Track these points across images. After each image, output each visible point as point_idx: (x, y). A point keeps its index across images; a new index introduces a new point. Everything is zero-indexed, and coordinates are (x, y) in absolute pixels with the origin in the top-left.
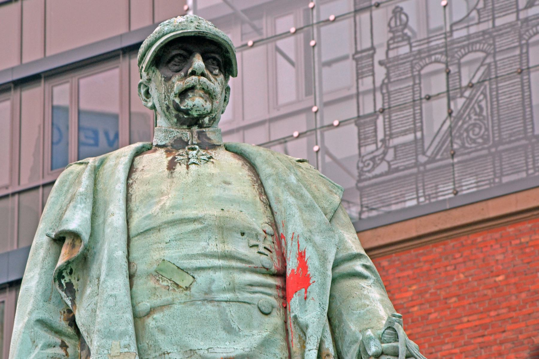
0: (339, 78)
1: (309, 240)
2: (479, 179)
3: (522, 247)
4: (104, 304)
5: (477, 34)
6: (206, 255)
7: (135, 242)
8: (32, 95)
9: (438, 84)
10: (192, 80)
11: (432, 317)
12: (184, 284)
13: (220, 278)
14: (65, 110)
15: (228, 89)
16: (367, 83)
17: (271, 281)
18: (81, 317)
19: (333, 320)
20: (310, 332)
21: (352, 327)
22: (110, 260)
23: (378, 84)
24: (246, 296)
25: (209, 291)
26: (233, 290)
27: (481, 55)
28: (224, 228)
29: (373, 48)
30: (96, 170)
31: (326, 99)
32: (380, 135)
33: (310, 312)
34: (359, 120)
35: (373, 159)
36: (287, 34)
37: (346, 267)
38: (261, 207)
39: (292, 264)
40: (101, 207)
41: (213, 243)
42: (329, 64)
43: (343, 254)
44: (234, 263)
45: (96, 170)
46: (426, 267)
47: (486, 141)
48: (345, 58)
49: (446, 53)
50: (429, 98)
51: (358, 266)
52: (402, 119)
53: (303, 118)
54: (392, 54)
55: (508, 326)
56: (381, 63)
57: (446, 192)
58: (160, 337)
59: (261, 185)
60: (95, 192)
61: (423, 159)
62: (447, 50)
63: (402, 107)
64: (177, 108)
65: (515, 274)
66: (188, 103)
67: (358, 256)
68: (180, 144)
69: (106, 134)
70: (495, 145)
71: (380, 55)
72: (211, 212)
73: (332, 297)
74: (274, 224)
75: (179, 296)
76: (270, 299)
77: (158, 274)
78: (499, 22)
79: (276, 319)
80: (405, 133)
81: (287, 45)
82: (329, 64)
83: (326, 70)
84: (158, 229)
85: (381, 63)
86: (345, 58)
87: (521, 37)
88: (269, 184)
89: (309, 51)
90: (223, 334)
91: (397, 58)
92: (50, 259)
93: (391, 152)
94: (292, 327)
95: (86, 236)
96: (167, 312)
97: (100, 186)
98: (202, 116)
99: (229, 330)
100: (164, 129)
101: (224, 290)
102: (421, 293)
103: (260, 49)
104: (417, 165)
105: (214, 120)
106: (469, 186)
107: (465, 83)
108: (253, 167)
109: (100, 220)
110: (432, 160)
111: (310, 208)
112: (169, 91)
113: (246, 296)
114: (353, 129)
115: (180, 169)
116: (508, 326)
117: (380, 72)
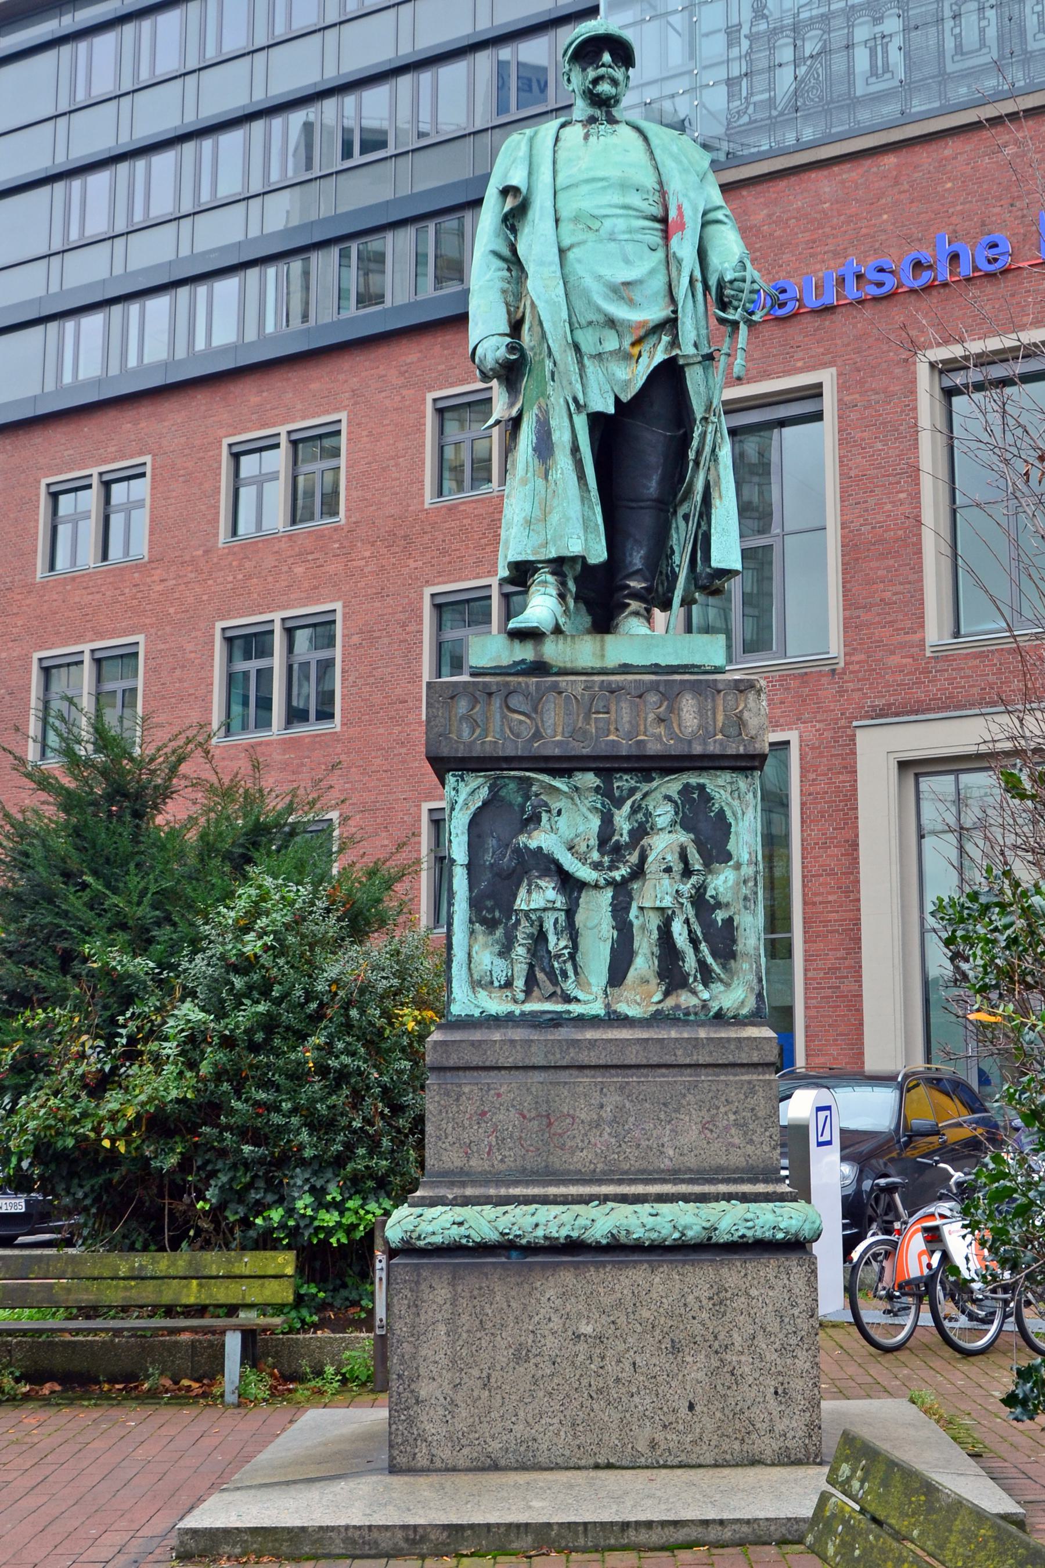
0: (714, 47)
1: (686, 195)
3: (843, 182)
4: (536, 242)
5: (817, 17)
6: (611, 206)
7: (559, 195)
8: (484, 59)
9: (787, 54)
10: (602, 71)
11: (777, 234)
12: (595, 227)
13: (621, 224)
14: (508, 63)
15: (628, 78)
16: (735, 52)
17: (658, 226)
18: (520, 252)
19: (702, 254)
20: (684, 264)
21: (715, 260)
22: (542, 207)
23: (743, 53)
24: (639, 237)
25: (612, 233)
26: (630, 232)
27: (820, 32)
28: (624, 186)
29: (740, 24)
30: (531, 140)
31: (704, 63)
32: (744, 94)
33: (685, 247)
34: (730, 82)
35: (738, 112)
36: (676, 11)
37: (711, 216)
38: (651, 170)
39: (673, 214)
40: (535, 167)
41: (616, 197)
42: (707, 35)
43: (708, 207)
44: (631, 212)
45: (531, 140)
46: (774, 196)
47: (821, 100)
48: (720, 31)
49: (794, 30)
50: (780, 65)
51: (719, 215)
52: (760, 81)
53: (686, 78)
54: (754, 30)
55: (829, 241)
56: (746, 37)
57: (790, 139)
58: (577, 266)
59: (652, 153)
60: (531, 156)
61: (774, 113)
62: (795, 28)
63: (760, 72)
64: (590, 91)
65: (837, 202)
67: (721, 207)
68: (592, 120)
69: (538, 81)
70: (828, 103)
71: (745, 30)
72: (614, 173)
73: (701, 238)
74: (661, 183)
75: (591, 236)
76: (656, 239)
77: (576, 219)
78: (833, 7)
79: (660, 254)
80: (762, 92)
81: (676, 20)
82: (707, 35)
83: (704, 39)
84: (576, 185)
85: (746, 37)
86: (720, 31)
87: (848, 20)
88: (657, 153)
89: (693, 26)
90: (622, 264)
91: (758, 33)
92: (498, 207)
93: (751, 107)
94: (672, 260)
95: (524, 190)
96: (582, 247)
97: (534, 152)
98: (609, 98)
99: (627, 261)
100: (581, 109)
101: (624, 232)
102: (770, 216)
103: (655, 24)
105: (617, 102)
106: (808, 134)
107: (807, 54)
108: (646, 139)
109: (534, 177)
110: (782, 114)
111: (685, 171)
112: (584, 79)
113: (639, 237)
114: (723, 89)
115: (593, 139)
116: (829, 241)
117: (745, 44)
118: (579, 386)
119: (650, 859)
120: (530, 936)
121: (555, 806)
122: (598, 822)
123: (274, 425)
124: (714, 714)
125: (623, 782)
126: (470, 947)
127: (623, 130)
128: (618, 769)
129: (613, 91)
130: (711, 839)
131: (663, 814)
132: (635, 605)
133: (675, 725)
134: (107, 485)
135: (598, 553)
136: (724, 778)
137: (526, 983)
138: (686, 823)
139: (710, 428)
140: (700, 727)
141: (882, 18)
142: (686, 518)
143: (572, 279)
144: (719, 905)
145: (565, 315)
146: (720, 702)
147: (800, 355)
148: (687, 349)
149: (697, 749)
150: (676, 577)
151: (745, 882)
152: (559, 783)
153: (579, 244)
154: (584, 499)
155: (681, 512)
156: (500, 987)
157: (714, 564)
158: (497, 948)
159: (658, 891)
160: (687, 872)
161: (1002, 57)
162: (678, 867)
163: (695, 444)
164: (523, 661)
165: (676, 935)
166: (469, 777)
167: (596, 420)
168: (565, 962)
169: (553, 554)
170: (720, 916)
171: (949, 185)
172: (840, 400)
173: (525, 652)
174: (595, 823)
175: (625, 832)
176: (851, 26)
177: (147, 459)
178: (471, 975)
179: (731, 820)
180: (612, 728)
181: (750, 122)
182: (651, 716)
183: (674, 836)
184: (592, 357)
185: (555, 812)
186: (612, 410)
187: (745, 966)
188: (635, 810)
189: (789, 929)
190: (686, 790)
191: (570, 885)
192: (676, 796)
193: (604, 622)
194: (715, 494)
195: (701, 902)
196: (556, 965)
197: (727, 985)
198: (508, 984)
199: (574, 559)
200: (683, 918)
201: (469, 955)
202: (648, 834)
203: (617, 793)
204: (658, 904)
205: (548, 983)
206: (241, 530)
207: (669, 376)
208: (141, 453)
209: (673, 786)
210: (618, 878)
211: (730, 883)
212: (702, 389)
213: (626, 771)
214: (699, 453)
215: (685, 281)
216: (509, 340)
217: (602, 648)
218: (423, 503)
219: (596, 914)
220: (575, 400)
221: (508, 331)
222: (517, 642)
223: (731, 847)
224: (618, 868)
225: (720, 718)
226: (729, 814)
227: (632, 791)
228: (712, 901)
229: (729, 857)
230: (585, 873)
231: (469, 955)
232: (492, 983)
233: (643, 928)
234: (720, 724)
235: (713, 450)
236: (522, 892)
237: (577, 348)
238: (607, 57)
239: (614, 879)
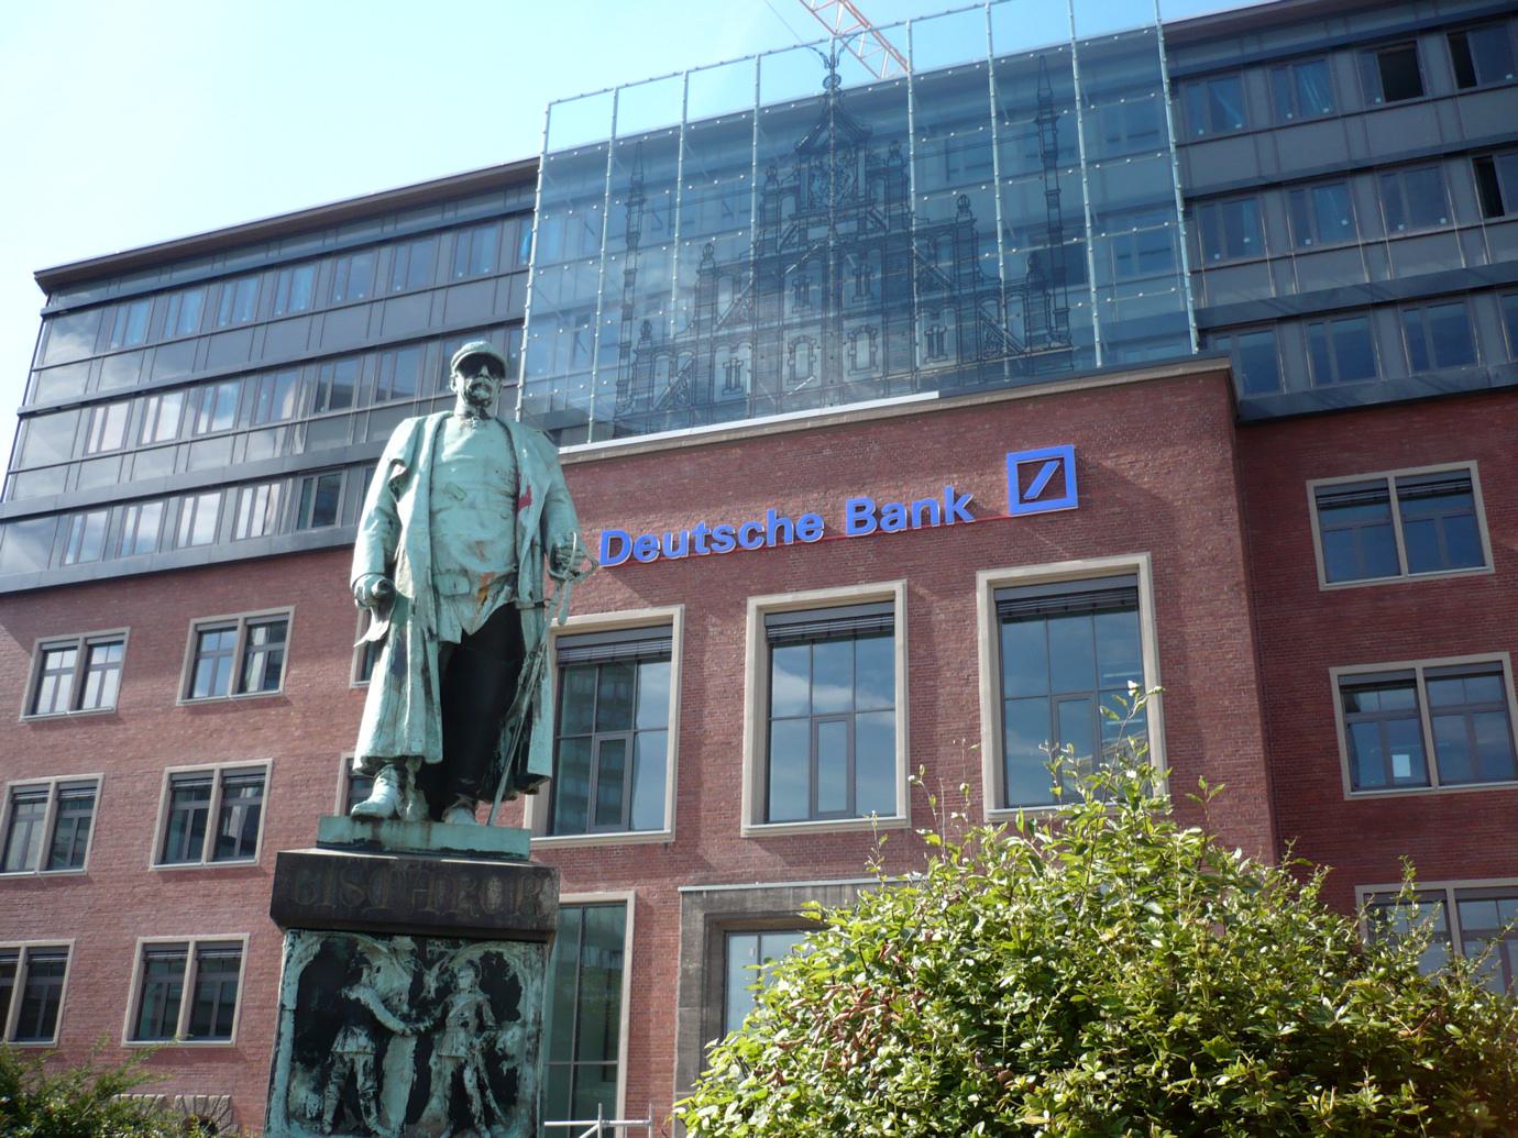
2: (807, 319)
10: (480, 380)
33: (529, 518)
39: (523, 492)
56: (635, 351)
66: (476, 392)
71: (634, 347)
75: (456, 504)
77: (446, 491)
104: (648, 412)
108: (509, 434)
117: (633, 356)
118: (434, 620)
119: (451, 1014)
120: (342, 1076)
121: (376, 964)
122: (410, 980)
123: (234, 612)
124: (515, 895)
125: (436, 947)
126: (290, 1082)
127: (493, 425)
128: (433, 932)
129: (488, 395)
130: (502, 995)
131: (466, 979)
132: (463, 799)
133: (482, 902)
134: (90, 648)
135: (436, 754)
136: (519, 948)
137: (334, 1118)
138: (485, 985)
139: (538, 661)
140: (501, 905)
141: (737, 347)
142: (512, 730)
143: (438, 536)
144: (506, 1057)
145: (428, 563)
146: (520, 885)
147: (657, 592)
148: (524, 596)
149: (499, 923)
150: (500, 776)
151: (529, 1038)
152: (381, 946)
153: (446, 509)
154: (429, 709)
155: (508, 726)
156: (312, 1119)
157: (530, 771)
158: (313, 1084)
159: (457, 1043)
160: (481, 1027)
161: (823, 385)
162: (473, 1023)
163: (524, 672)
164: (363, 840)
165: (466, 1082)
166: (305, 934)
167: (446, 647)
168: (369, 1100)
169: (398, 753)
170: (506, 1066)
171: (780, 474)
172: (686, 629)
173: (364, 832)
174: (407, 980)
175: (432, 990)
176: (713, 352)
177: (127, 630)
178: (287, 1108)
179: (522, 984)
180: (429, 902)
181: (632, 414)
182: (463, 894)
183: (472, 996)
184: (447, 597)
185: (375, 969)
186: (458, 640)
187: (523, 1111)
188: (443, 971)
189: (615, 1057)
190: (487, 957)
191: (380, 1035)
192: (477, 961)
193: (436, 813)
194: (536, 714)
195: (493, 1057)
196: (362, 1102)
197: (507, 1127)
198: (319, 1117)
199: (415, 758)
200: (473, 1067)
201: (288, 1089)
202: (451, 992)
203: (429, 956)
204: (454, 1053)
205: (353, 1118)
206: (197, 694)
207: (506, 622)
208: (122, 625)
209: (475, 952)
210: (422, 1029)
211: (517, 1039)
212: (533, 630)
213: (438, 937)
214: (526, 679)
215: (527, 544)
216: (383, 578)
217: (429, 833)
218: (348, 684)
219: (401, 1060)
220: (430, 630)
221: (383, 571)
222: (358, 823)
223: (520, 1007)
224: (424, 1021)
225: (520, 898)
226: (520, 979)
227: (442, 955)
228: (500, 1053)
229: (517, 1015)
230: (393, 1023)
231: (288, 1089)
232: (305, 1115)
233: (440, 1073)
234: (518, 903)
235: (538, 678)
236: (340, 1037)
237: (435, 589)
238: (485, 371)
239: (418, 1029)
